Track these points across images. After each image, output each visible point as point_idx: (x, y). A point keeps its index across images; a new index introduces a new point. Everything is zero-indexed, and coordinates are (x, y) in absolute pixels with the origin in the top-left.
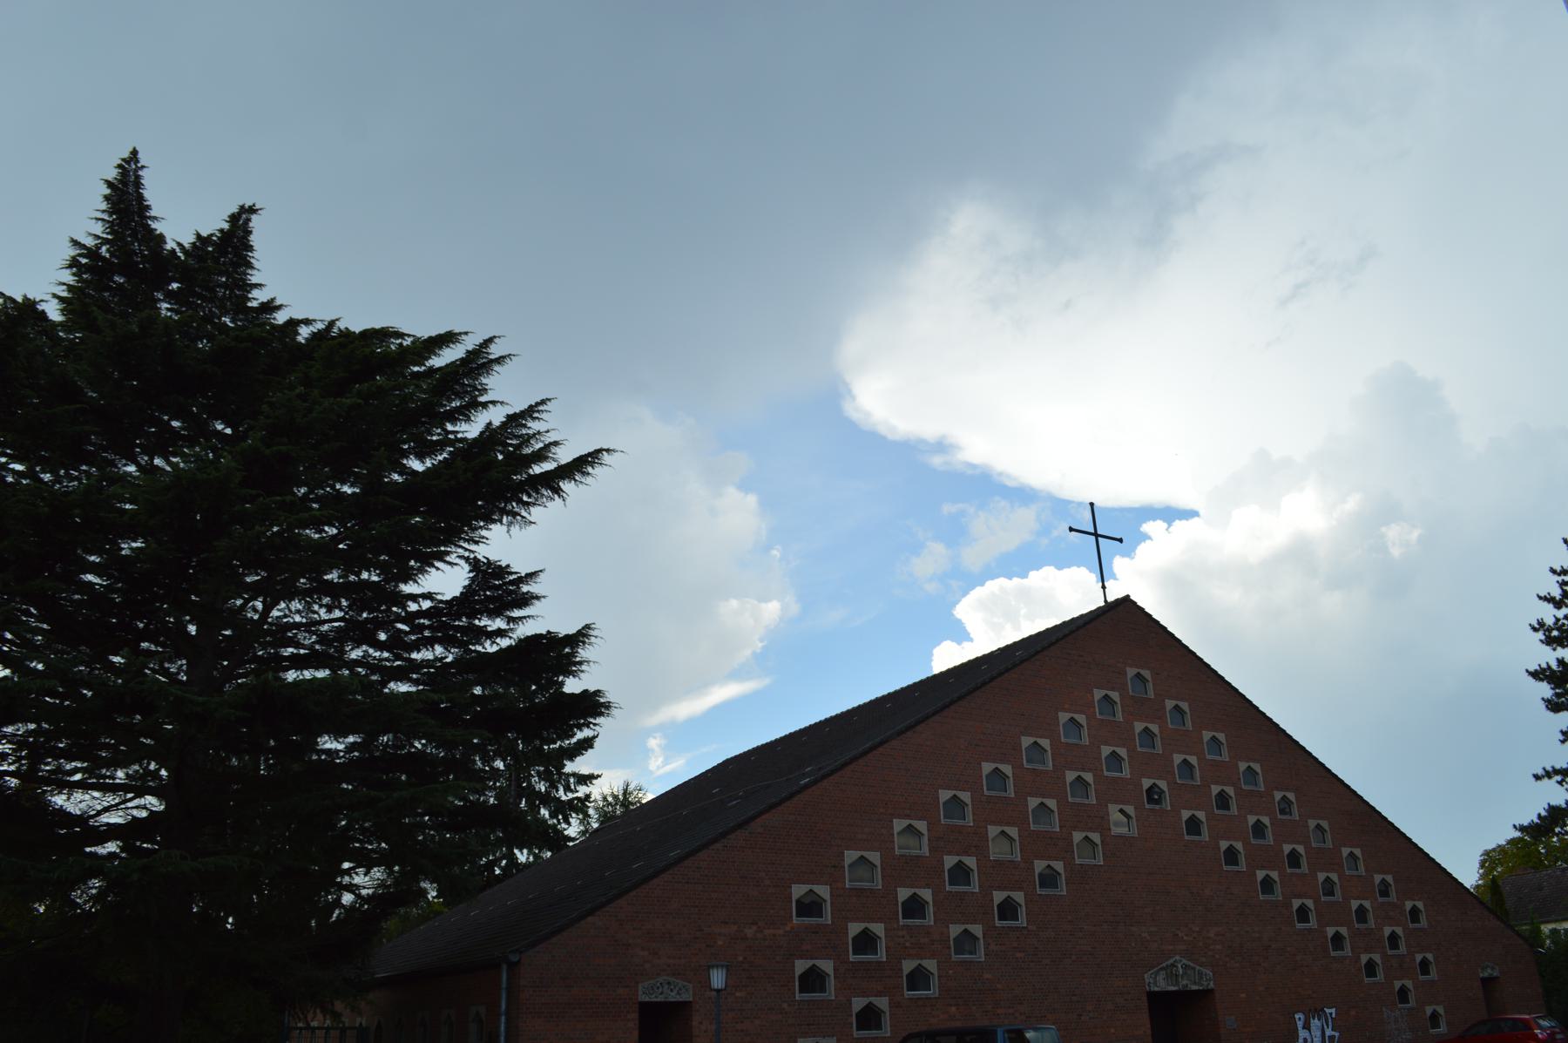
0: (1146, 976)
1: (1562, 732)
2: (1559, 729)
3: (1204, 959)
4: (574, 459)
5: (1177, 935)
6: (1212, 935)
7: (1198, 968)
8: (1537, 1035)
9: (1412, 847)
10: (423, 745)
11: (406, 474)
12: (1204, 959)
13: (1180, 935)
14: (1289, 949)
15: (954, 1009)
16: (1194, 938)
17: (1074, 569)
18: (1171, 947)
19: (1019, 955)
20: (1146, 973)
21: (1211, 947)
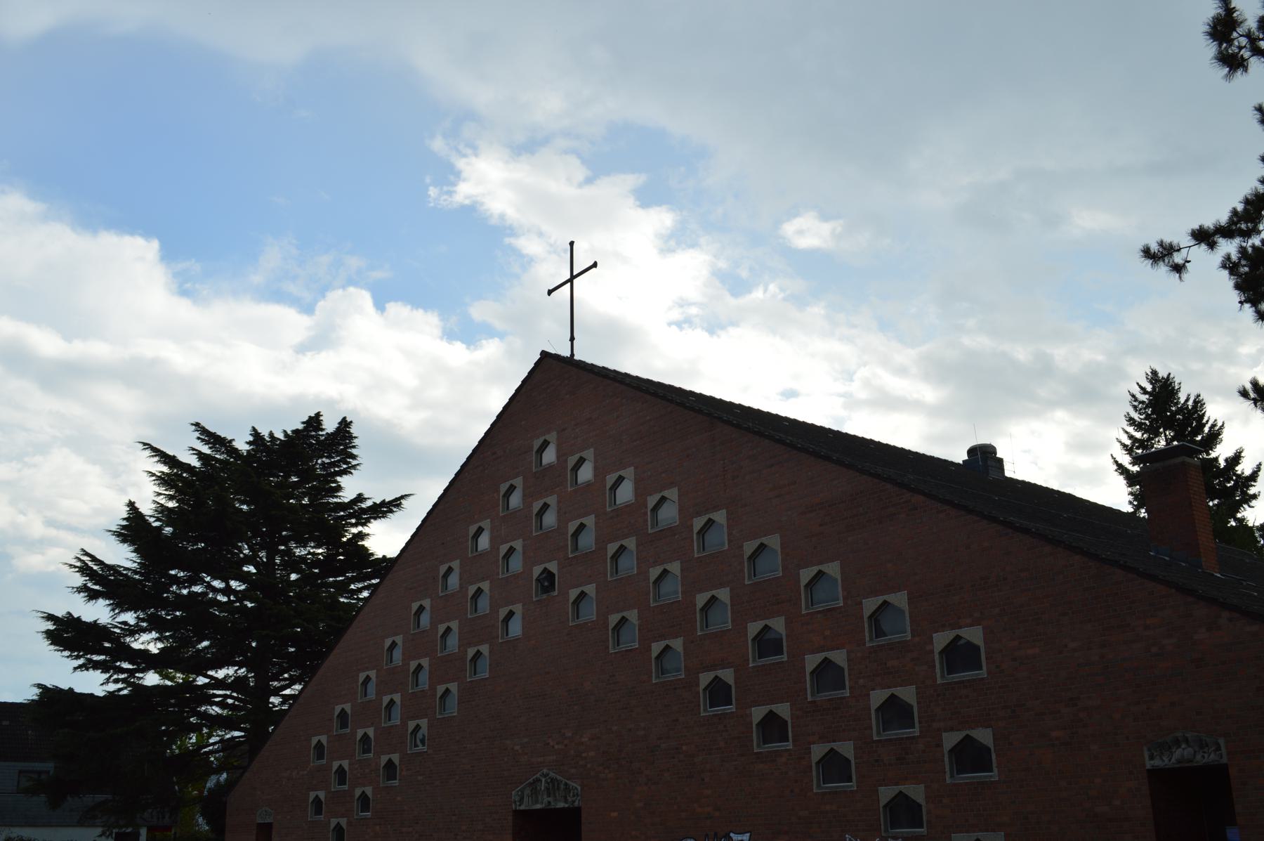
0: (513, 793)
1: (255, 433)
2: (1223, 82)
3: (573, 771)
4: (648, 380)
5: (548, 744)
6: (585, 740)
7: (538, 775)
8: (146, 652)
9: (405, 554)
10: (190, 677)
11: (368, 512)
12: (573, 771)
13: (551, 744)
14: (684, 748)
15: (378, 827)
16: (566, 745)
17: (184, 461)
18: (540, 759)
19: (420, 778)
20: (514, 790)
21: (584, 755)
